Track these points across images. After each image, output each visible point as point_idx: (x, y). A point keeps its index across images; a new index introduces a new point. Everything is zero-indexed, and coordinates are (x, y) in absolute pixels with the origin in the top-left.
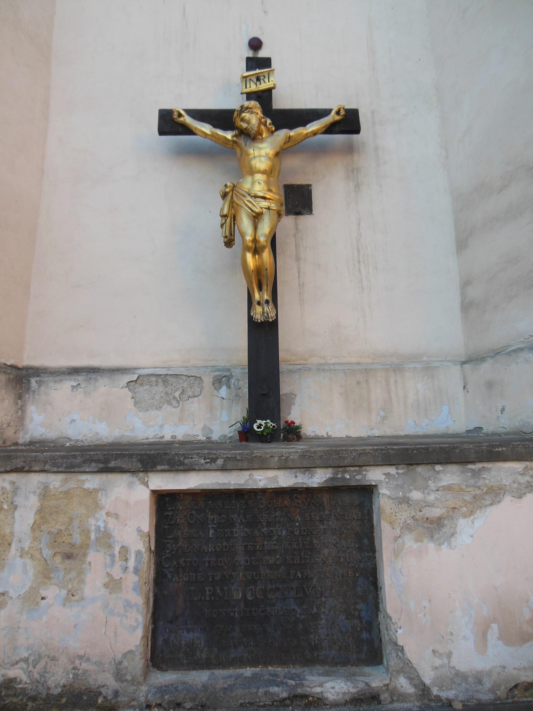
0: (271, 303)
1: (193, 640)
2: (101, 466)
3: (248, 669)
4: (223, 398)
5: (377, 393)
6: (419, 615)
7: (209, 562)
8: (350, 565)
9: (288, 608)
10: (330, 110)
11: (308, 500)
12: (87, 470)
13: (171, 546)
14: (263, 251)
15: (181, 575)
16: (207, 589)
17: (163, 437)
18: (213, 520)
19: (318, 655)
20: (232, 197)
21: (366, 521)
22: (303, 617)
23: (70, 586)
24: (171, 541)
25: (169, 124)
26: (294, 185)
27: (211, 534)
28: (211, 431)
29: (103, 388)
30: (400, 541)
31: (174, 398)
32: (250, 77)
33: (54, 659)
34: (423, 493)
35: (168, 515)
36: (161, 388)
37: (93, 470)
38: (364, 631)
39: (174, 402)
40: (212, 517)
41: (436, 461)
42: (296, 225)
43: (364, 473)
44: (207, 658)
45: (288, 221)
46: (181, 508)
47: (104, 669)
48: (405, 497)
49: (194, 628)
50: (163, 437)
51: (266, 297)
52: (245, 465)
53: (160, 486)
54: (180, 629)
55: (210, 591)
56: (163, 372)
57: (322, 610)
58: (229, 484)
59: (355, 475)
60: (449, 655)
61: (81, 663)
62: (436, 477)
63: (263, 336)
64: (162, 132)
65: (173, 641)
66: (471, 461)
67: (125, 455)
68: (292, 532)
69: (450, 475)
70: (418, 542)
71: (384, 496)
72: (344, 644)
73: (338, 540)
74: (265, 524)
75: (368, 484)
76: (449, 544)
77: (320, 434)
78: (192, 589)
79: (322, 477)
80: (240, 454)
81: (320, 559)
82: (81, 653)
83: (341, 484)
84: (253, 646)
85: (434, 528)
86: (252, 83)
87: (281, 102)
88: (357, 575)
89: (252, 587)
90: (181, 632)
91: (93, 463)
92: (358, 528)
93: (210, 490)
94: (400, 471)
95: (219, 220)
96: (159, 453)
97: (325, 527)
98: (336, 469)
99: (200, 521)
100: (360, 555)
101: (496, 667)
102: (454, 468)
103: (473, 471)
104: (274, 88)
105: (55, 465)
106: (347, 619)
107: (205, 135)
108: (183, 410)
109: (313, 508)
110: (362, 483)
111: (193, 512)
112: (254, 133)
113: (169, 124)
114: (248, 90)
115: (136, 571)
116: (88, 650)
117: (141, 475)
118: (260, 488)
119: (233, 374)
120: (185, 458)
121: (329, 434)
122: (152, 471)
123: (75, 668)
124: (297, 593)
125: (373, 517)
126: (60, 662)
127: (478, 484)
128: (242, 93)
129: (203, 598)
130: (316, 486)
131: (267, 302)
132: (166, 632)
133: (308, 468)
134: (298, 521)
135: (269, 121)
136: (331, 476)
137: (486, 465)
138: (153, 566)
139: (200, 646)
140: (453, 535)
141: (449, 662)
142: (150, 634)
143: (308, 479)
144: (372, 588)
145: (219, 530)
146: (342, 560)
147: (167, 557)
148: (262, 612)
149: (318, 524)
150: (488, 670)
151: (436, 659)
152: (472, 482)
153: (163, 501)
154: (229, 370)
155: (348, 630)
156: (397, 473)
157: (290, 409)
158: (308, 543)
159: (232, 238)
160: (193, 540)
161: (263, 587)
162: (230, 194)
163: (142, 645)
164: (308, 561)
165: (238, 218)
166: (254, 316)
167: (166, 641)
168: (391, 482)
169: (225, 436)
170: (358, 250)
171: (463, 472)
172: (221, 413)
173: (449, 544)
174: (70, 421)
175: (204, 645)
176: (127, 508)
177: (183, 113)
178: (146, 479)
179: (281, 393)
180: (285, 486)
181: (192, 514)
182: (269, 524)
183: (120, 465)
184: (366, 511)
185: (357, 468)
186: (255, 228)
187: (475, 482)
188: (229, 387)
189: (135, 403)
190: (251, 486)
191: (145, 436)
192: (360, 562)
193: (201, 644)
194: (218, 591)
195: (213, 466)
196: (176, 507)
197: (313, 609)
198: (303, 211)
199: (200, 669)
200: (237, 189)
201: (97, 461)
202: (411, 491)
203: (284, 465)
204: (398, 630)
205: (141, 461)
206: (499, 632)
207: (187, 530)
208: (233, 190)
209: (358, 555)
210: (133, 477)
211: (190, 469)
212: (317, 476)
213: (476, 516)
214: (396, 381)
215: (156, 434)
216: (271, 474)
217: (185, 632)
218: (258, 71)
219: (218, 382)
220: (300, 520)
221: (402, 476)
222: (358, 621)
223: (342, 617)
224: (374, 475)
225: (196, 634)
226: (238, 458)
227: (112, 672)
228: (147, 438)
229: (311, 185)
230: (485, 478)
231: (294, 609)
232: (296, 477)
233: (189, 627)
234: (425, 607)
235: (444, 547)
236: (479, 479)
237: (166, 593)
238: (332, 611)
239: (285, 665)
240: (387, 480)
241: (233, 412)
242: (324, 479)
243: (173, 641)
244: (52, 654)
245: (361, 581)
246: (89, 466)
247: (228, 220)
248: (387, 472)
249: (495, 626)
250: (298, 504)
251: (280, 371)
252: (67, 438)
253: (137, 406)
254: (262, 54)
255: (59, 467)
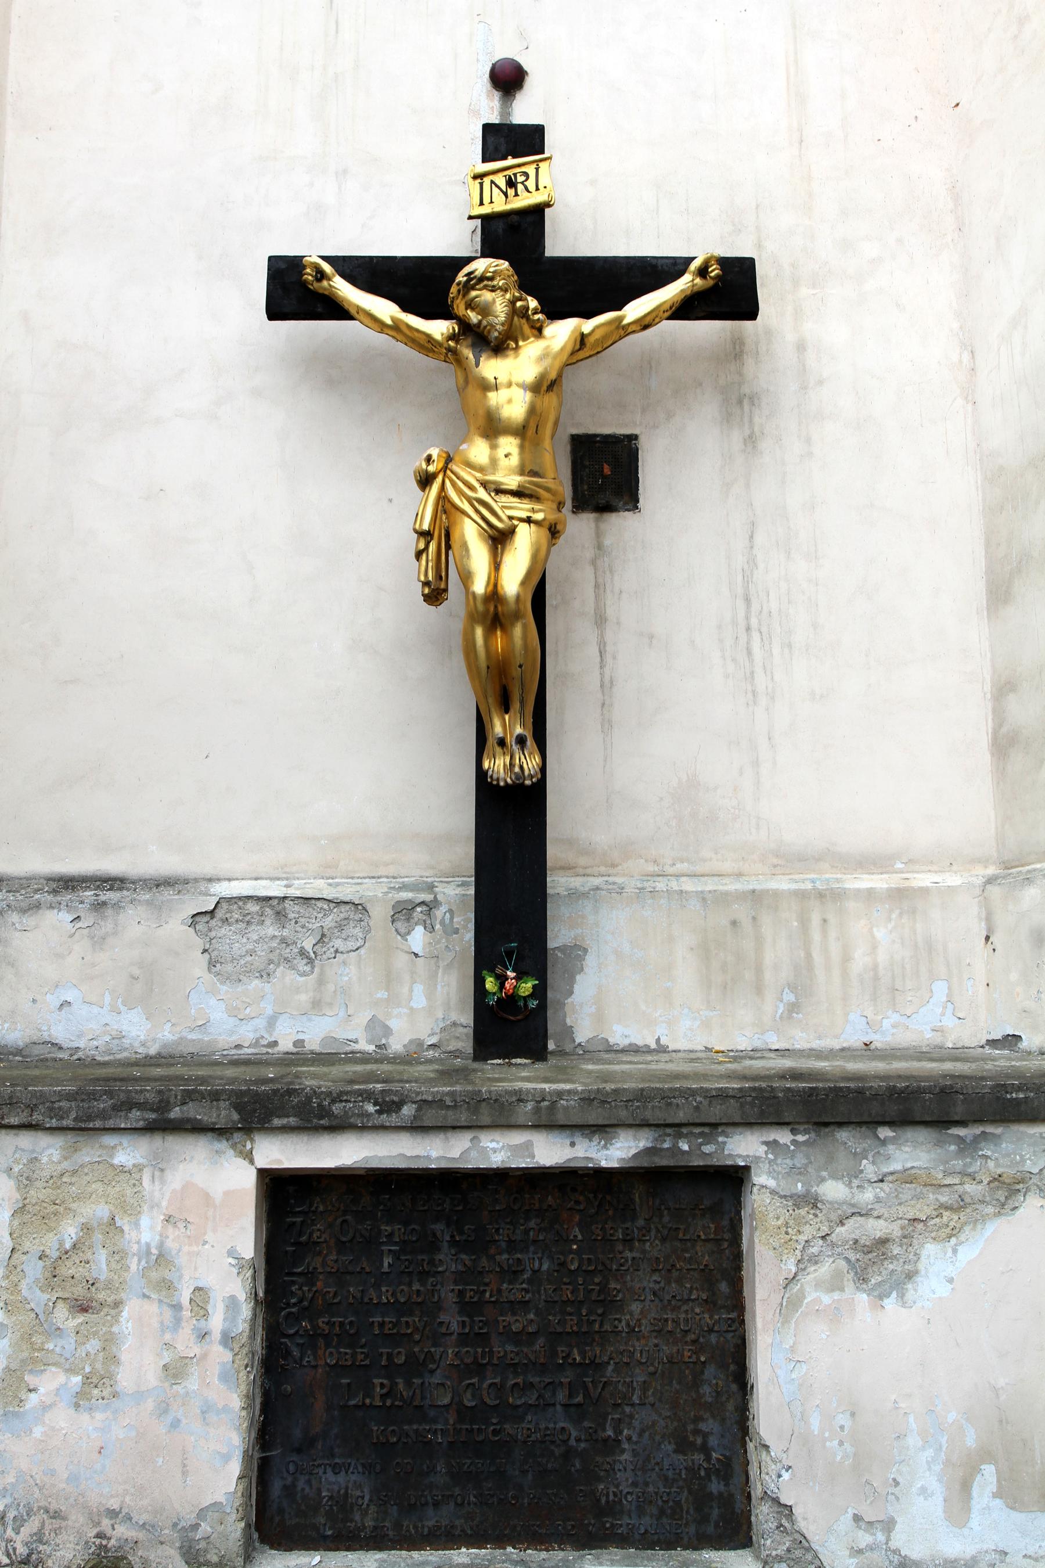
0: (530, 742)
1: (347, 1488)
2: (153, 1116)
3: (464, 1550)
4: (416, 955)
5: (778, 951)
6: (828, 1444)
7: (382, 1325)
8: (688, 1339)
9: (551, 1425)
10: (690, 260)
11: (600, 1196)
12: (123, 1126)
13: (300, 1289)
14: (513, 625)
15: (320, 1352)
16: (376, 1381)
17: (275, 1043)
18: (391, 1235)
19: (612, 1525)
20: (443, 482)
21: (726, 1245)
22: (583, 1445)
23: (88, 1369)
24: (300, 1280)
25: (294, 292)
26: (596, 435)
27: (386, 1264)
28: (388, 1031)
29: (133, 922)
30: (796, 1288)
31: (303, 953)
32: (491, 177)
33: (56, 1515)
34: (849, 1185)
35: (294, 1223)
36: (271, 929)
37: (134, 1125)
38: (713, 1478)
39: (302, 965)
40: (389, 1228)
41: (880, 1119)
42: (599, 534)
43: (720, 1139)
44: (375, 1528)
45: (580, 527)
46: (321, 1208)
47: (162, 1540)
48: (808, 1192)
49: (349, 1464)
50: (275, 1043)
51: (519, 730)
52: (463, 1118)
53: (280, 1161)
54: (320, 1465)
55: (382, 1385)
56: (275, 890)
57: (625, 1432)
58: (428, 1157)
59: (701, 1144)
60: (888, 1526)
61: (113, 1526)
62: (878, 1152)
63: (511, 823)
64: (275, 312)
65: (303, 1490)
66: (956, 1118)
67: (202, 1096)
68: (563, 1264)
69: (911, 1152)
70: (833, 1290)
71: (764, 1190)
72: (671, 1504)
73: (662, 1284)
74: (503, 1245)
75: (729, 1163)
76: (902, 1296)
77: (640, 1043)
78: (344, 1381)
79: (630, 1147)
80: (449, 1093)
81: (624, 1323)
82: (114, 1504)
83: (671, 1163)
84: (475, 1504)
85: (878, 1265)
86: (495, 190)
87: (564, 240)
88: (703, 1359)
89: (474, 1380)
90: (321, 1471)
91: (134, 1111)
92: (707, 1257)
93: (386, 1169)
94: (800, 1138)
95: (412, 543)
96: (278, 1090)
97: (635, 1254)
98: (661, 1131)
99: (362, 1236)
100: (711, 1318)
101: (986, 1552)
102: (922, 1134)
103: (961, 1139)
104: (548, 205)
105: (52, 1113)
106: (675, 1451)
107: (380, 325)
108: (321, 982)
109: (611, 1213)
110: (715, 1162)
111: (348, 1217)
112: (496, 338)
113: (294, 292)
114: (486, 210)
115: (227, 1339)
116: (127, 1499)
117: (237, 1136)
118: (495, 1166)
119: (440, 897)
120: (333, 1101)
121: (664, 1041)
122: (259, 1130)
123: (99, 1536)
124: (570, 1396)
125: (740, 1236)
126: (70, 1523)
127: (971, 1170)
128: (470, 218)
129: (368, 1401)
130: (616, 1165)
131: (521, 741)
132: (288, 1472)
133: (602, 1130)
134: (575, 1241)
135: (533, 303)
136: (650, 1145)
137: (990, 1129)
138: (260, 1332)
139: (360, 1502)
140: (910, 1276)
141: (888, 1539)
142: (255, 1473)
143: (598, 1151)
144: (734, 1387)
145: (403, 1258)
146: (670, 1326)
147: (290, 1313)
148: (495, 1432)
149: (621, 1248)
150: (968, 1556)
151: (861, 1533)
152: (958, 1164)
153: (280, 1191)
154: (431, 888)
155: (680, 1474)
156: (794, 1142)
157: (572, 981)
158: (598, 1288)
159: (443, 586)
160: (348, 1277)
161: (497, 1380)
162: (440, 477)
163: (240, 1494)
164: (597, 1327)
165: (455, 536)
166: (490, 773)
167: (289, 1491)
168: (779, 1161)
169: (420, 1043)
170: (748, 600)
171: (939, 1144)
172: (411, 990)
173: (902, 1296)
174: (58, 1004)
175: (370, 1500)
176: (200, 1215)
177: (327, 268)
178: (249, 1146)
179: (551, 944)
180: (548, 1165)
181: (344, 1221)
182: (512, 1245)
183: (192, 1114)
184: (725, 1222)
185: (707, 1130)
186: (496, 566)
187: (965, 1165)
188: (430, 929)
189: (212, 964)
190: (475, 1162)
191: (234, 1039)
192: (711, 1331)
193: (363, 1498)
194: (401, 1387)
195: (393, 1119)
196: (311, 1206)
197: (604, 1430)
198: (614, 502)
199: (361, 1548)
200: (455, 468)
201: (141, 1106)
202: (823, 1180)
203: (549, 1120)
204: (783, 1472)
205: (238, 1107)
206: (998, 1481)
207: (333, 1257)
208: (445, 468)
209: (707, 1316)
210: (219, 1141)
211: (338, 1126)
212: (618, 1145)
213: (962, 1237)
214: (825, 921)
215: (258, 1036)
216: (517, 1138)
217: (329, 1470)
218: (510, 161)
219: (403, 912)
220: (580, 1237)
221: (803, 1148)
222: (702, 1457)
223: (668, 1447)
224: (743, 1147)
225: (353, 1477)
226: (449, 1103)
227: (177, 1545)
228: (238, 1047)
229: (635, 437)
230: (987, 1157)
231: (563, 1428)
232: (573, 1144)
233: (337, 1460)
234: (842, 1427)
235: (890, 1303)
236: (972, 1158)
237: (289, 1388)
238: (647, 1434)
239: (541, 1543)
240: (770, 1156)
241: (439, 987)
242: (633, 1151)
243: (303, 1490)
244: (54, 1506)
245: (710, 1371)
246: (127, 1118)
247: (433, 547)
248: (771, 1139)
249: (989, 1471)
250: (577, 1202)
251: (549, 891)
252: (53, 1044)
253: (214, 969)
254: (524, 111)
255: (62, 1118)
